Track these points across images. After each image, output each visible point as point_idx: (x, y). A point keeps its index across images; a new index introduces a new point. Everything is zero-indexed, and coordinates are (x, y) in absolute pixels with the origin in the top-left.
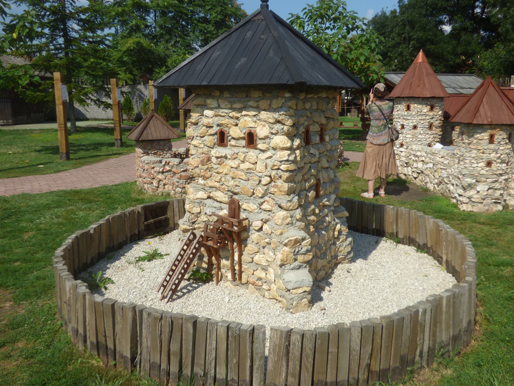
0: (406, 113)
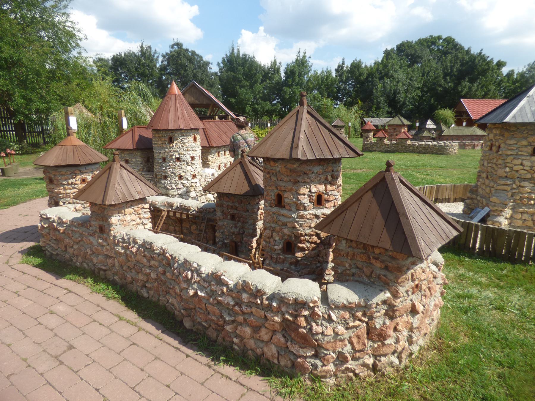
0: (194, 144)
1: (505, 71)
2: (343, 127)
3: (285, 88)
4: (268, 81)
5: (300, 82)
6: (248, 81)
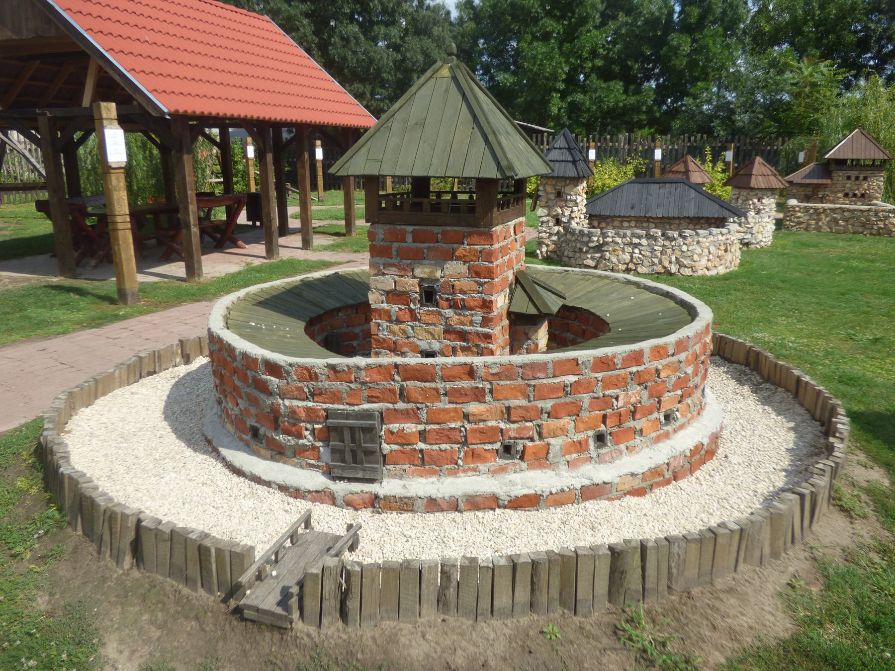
1: (792, 424)
2: (876, 166)
3: (675, 39)
4: (622, 17)
5: (730, 13)
6: (558, 19)
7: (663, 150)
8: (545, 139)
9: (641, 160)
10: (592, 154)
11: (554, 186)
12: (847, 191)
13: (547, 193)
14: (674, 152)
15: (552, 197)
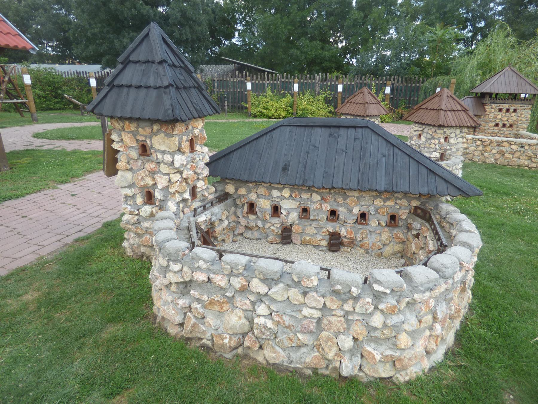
7: (344, 85)
8: (266, 76)
9: (329, 92)
10: (296, 87)
11: (135, 134)
12: (498, 121)
13: (127, 147)
14: (351, 87)
15: (134, 154)
